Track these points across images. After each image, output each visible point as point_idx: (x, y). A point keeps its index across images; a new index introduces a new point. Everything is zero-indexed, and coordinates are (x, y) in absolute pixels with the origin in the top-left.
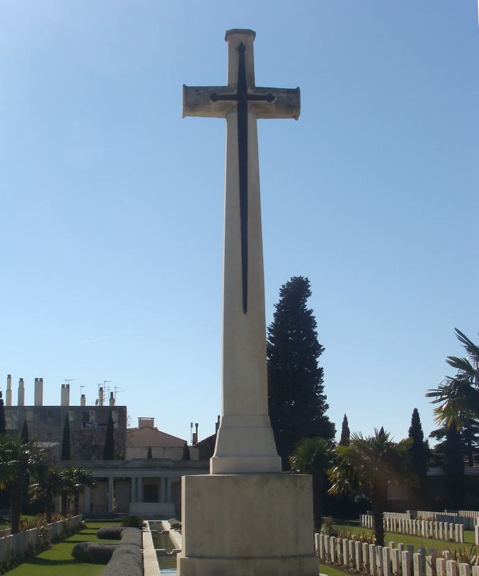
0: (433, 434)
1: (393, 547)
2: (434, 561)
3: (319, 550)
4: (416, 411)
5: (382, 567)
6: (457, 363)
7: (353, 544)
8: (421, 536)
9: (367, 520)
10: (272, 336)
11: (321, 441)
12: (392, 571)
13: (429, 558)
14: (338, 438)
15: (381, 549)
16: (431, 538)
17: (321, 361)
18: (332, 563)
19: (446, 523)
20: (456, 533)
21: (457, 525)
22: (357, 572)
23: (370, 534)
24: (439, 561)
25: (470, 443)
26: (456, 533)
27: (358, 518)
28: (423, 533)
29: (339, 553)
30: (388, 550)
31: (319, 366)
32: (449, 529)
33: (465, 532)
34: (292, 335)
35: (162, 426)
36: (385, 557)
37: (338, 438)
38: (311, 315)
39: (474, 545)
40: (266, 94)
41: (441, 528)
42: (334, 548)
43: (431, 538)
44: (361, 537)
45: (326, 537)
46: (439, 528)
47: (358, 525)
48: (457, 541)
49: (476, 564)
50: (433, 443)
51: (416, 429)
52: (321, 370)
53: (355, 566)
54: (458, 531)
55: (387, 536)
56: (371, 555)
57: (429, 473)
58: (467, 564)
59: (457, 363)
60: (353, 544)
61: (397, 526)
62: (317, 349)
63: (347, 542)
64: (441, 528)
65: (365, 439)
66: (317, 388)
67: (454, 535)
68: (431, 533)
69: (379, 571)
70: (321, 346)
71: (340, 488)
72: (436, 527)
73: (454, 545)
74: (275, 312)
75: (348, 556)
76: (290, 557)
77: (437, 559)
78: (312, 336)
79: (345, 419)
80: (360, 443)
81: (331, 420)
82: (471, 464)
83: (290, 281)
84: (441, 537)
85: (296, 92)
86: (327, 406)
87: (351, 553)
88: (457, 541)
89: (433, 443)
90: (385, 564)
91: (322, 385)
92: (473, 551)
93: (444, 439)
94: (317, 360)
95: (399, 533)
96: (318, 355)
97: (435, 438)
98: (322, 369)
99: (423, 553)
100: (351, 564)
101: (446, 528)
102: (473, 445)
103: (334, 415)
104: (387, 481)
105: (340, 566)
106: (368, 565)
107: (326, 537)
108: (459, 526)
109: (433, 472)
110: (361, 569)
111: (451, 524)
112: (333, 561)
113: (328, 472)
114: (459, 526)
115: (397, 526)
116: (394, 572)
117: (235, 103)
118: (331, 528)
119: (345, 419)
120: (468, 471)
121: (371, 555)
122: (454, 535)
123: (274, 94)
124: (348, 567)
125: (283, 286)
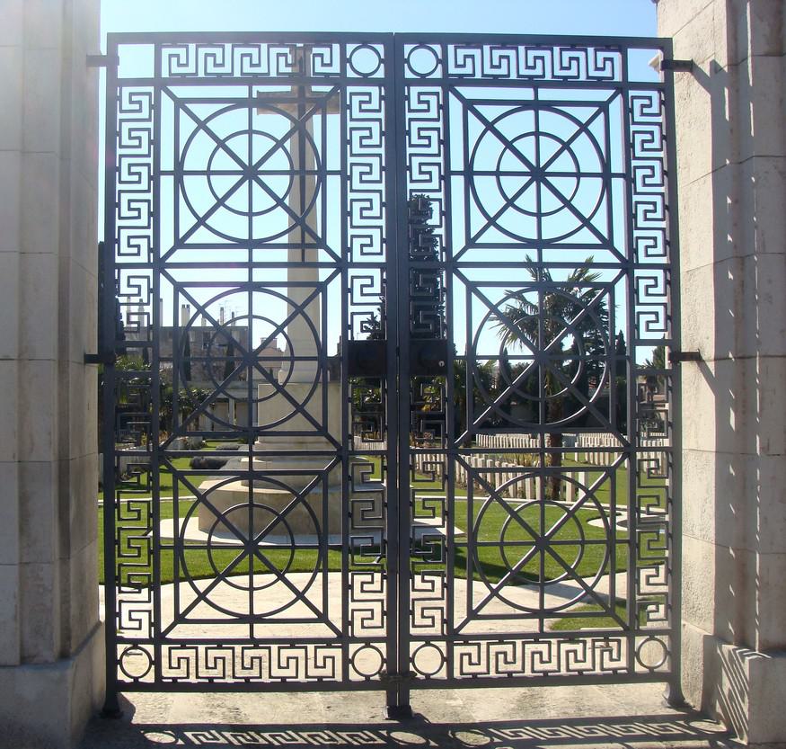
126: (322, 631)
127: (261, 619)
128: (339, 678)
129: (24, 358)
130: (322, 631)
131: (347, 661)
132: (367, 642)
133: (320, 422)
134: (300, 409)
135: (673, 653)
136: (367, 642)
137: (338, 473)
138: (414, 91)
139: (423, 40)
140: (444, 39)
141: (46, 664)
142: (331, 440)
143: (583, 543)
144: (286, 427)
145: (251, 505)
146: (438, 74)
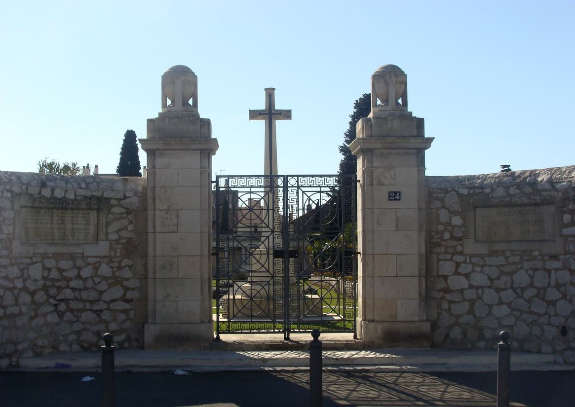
35: (516, 168)
40: (279, 112)
74: (350, 121)
77: (519, 312)
83: (362, 97)
85: (290, 111)
117: (267, 116)
123: (282, 112)
125: (357, 101)
126: (304, 189)
127: (318, 192)
128: (299, 178)
129: (202, 256)
130: (304, 189)
131: (297, 182)
132: (293, 186)
133: (268, 269)
134: (263, 266)
135: (355, 326)
136: (293, 186)
137: (272, 282)
138: (290, 189)
139: (292, 176)
140: (298, 176)
141: (206, 323)
142: (271, 274)
143: (331, 298)
144: (260, 270)
145: (251, 289)
146: (296, 185)
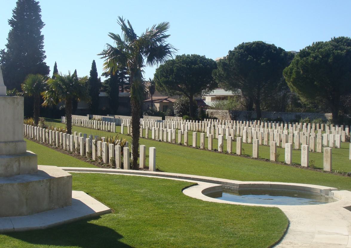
0: (103, 75)
1: (76, 135)
2: (96, 142)
3: (37, 136)
4: (94, 61)
5: (69, 145)
6: (116, 37)
7: (55, 133)
8: (93, 129)
9: (64, 119)
10: (15, 15)
11: (40, 76)
12: (74, 147)
13: (94, 141)
14: (51, 75)
15: (69, 136)
16: (98, 129)
17: (43, 31)
18: (43, 143)
19: (106, 122)
20: (112, 127)
21: (112, 123)
22: (57, 148)
23: (64, 127)
24: (99, 142)
25: (123, 80)
26: (112, 127)
27: (60, 118)
28: (95, 127)
29: (47, 137)
30: (73, 136)
31: (42, 34)
32: (108, 124)
33: (116, 126)
34: (27, 15)
36: (71, 140)
37: (51, 75)
38: (38, 5)
39: (120, 133)
41: (104, 124)
42: (45, 135)
43: (98, 129)
44: (59, 129)
45: (41, 128)
46: (103, 124)
47: (60, 122)
48: (112, 131)
49: (118, 144)
50: (103, 79)
51: (94, 72)
52: (43, 36)
53: (55, 145)
54: (112, 126)
55: (73, 128)
56: (64, 138)
57: (100, 95)
58: (113, 144)
59: (116, 37)
60: (55, 133)
61: (81, 123)
62: (41, 24)
63: (52, 132)
64: (104, 124)
65: (63, 76)
66: (40, 46)
67: (110, 128)
68: (99, 127)
69: (68, 147)
70: (43, 23)
71: (48, 102)
72: (101, 124)
73: (109, 134)
75: (52, 139)
76: (10, 142)
78: (38, 17)
79: (56, 64)
80: (61, 79)
81: (47, 65)
82: (122, 91)
84: (104, 129)
86: (45, 57)
87: (53, 138)
88: (112, 131)
89: (103, 79)
90: (71, 144)
91: (43, 45)
92: (117, 138)
93: (109, 77)
94: (41, 30)
95: (82, 127)
96: (41, 28)
97: (105, 76)
98: (43, 36)
99: (92, 138)
100: (53, 144)
101: (106, 124)
102: (124, 81)
103: (49, 62)
104: (137, 73)
105: (47, 144)
106: (62, 144)
107: (41, 128)
108: (113, 124)
109: (102, 94)
110: (59, 146)
111: (109, 123)
112: (44, 141)
113: (42, 94)
114: (113, 124)
115: (81, 123)
116: (75, 148)
118: (43, 124)
119: (56, 64)
120: (121, 94)
121: (64, 138)
122: (110, 128)
124: (51, 145)
